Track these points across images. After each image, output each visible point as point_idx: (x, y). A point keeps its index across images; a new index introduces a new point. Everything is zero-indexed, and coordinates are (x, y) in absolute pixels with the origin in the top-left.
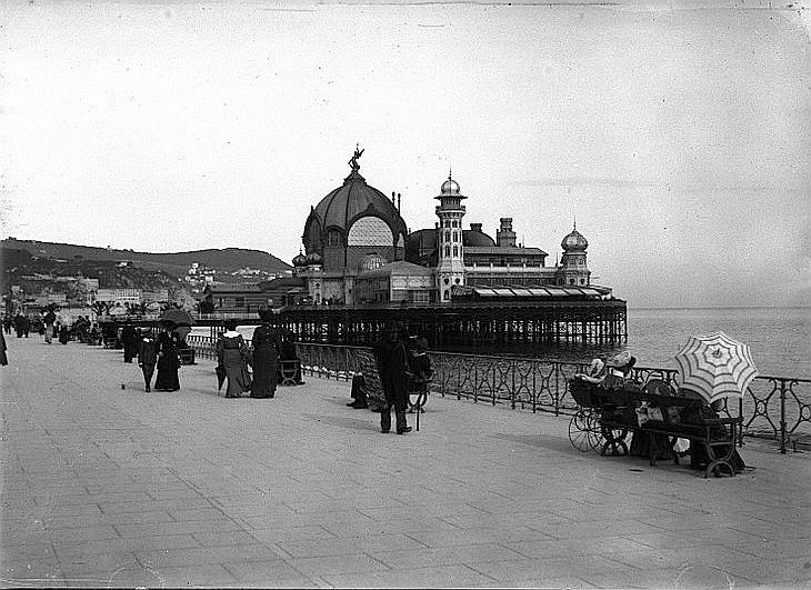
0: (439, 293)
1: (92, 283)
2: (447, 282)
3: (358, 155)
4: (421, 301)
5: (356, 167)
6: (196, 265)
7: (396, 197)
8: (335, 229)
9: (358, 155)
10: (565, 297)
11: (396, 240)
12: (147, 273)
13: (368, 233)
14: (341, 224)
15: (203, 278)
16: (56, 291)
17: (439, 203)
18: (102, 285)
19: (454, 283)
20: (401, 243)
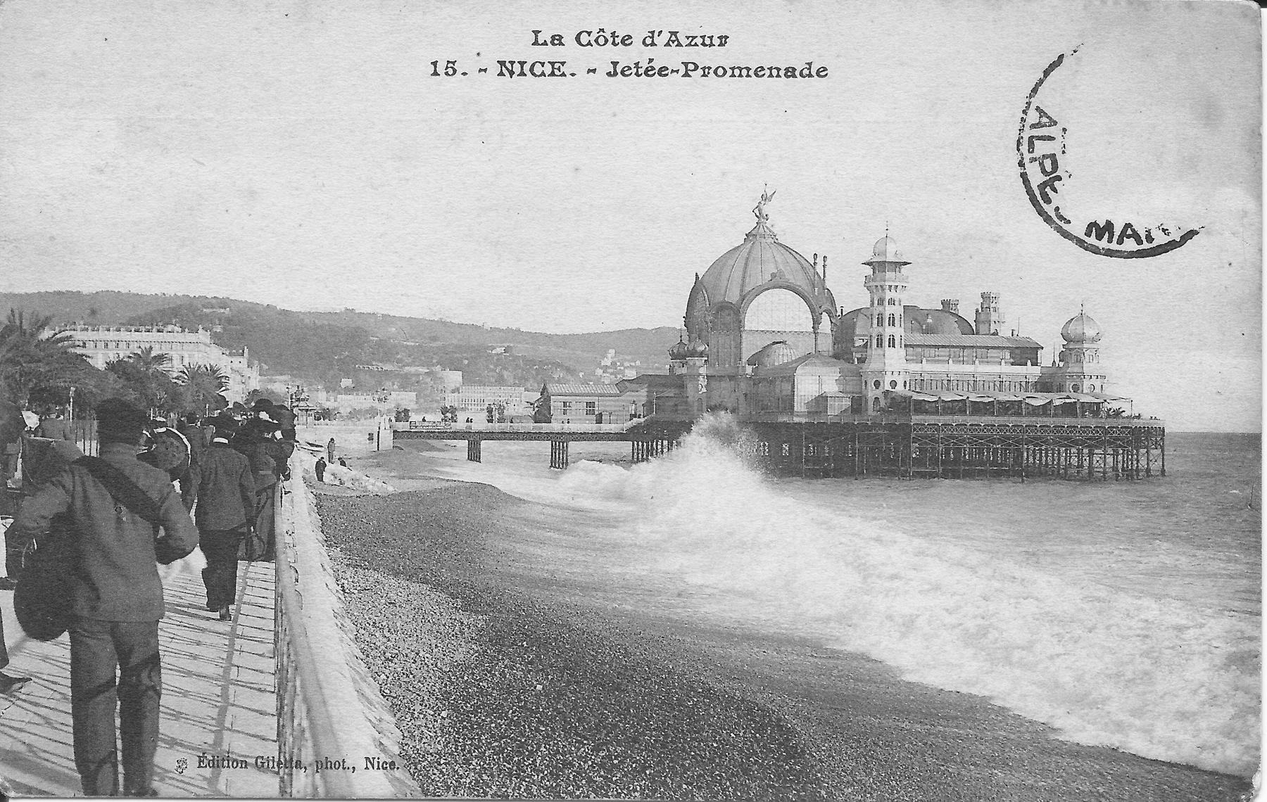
0: (866, 402)
1: (455, 377)
2: (877, 384)
3: (765, 198)
4: (837, 409)
5: (760, 216)
6: (612, 352)
7: (820, 261)
8: (724, 307)
9: (765, 198)
10: (132, 508)
11: (816, 322)
12: (533, 362)
13: (776, 316)
14: (733, 296)
15: (622, 372)
16: (403, 387)
17: (868, 270)
18: (467, 380)
19: (888, 387)
20: (826, 325)
